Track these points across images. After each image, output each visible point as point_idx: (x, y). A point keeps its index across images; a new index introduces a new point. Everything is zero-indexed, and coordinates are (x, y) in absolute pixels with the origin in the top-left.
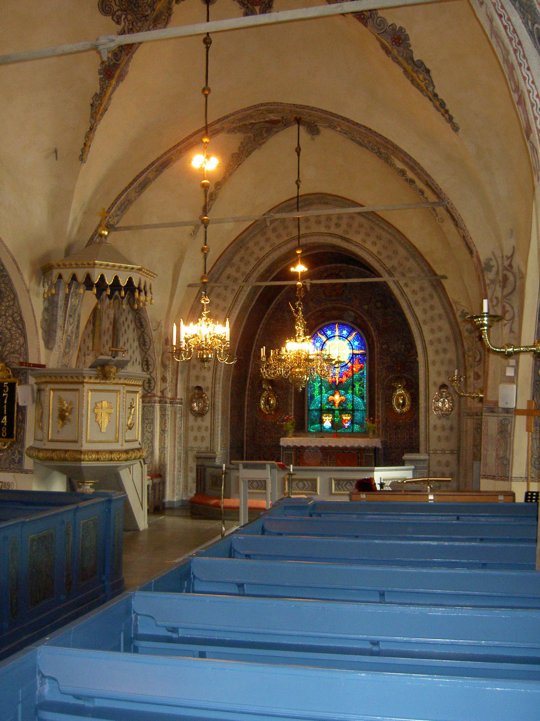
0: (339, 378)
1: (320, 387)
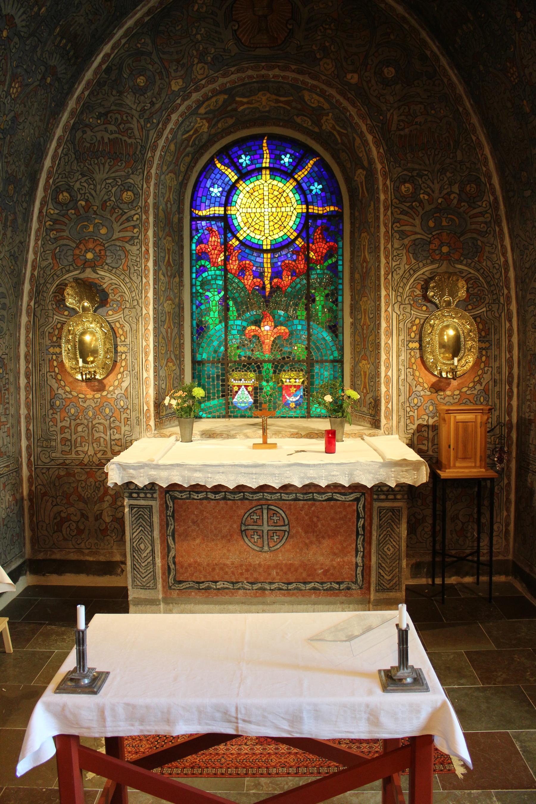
0: (271, 279)
1: (225, 299)
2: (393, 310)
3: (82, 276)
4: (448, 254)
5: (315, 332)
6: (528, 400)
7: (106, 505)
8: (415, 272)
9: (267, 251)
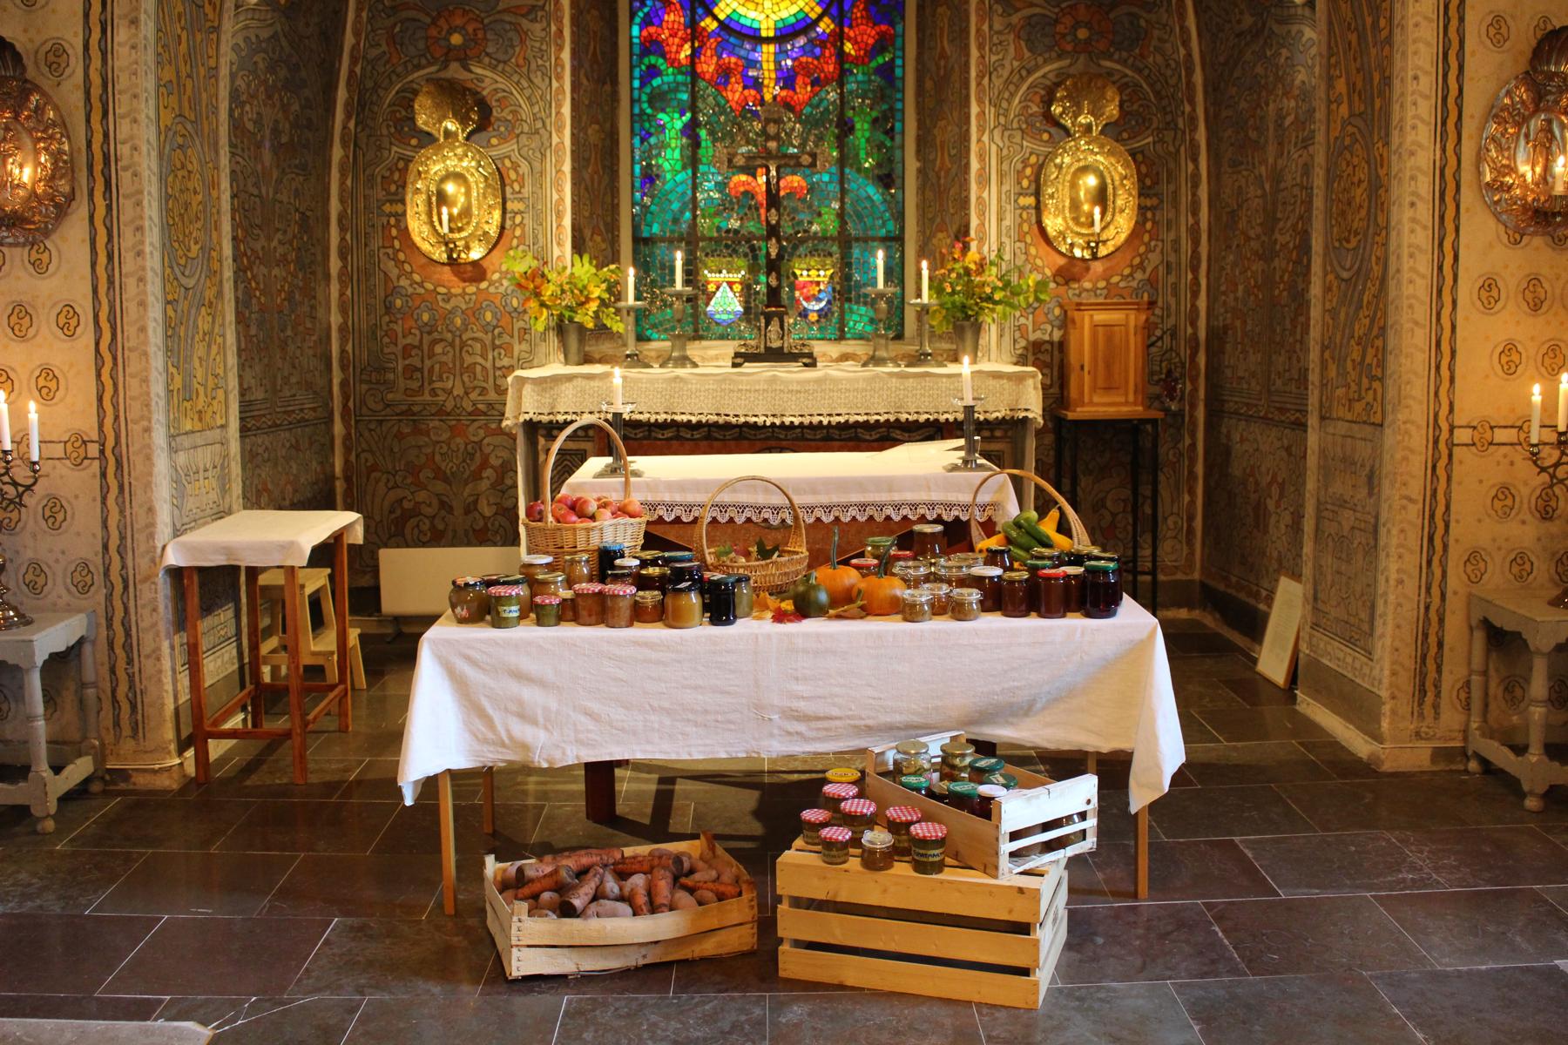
1: (690, 130)
2: (992, 139)
3: (443, 75)
4: (1088, 41)
5: (854, 186)
6: (1224, 293)
7: (484, 485)
8: (1029, 73)
9: (768, 40)
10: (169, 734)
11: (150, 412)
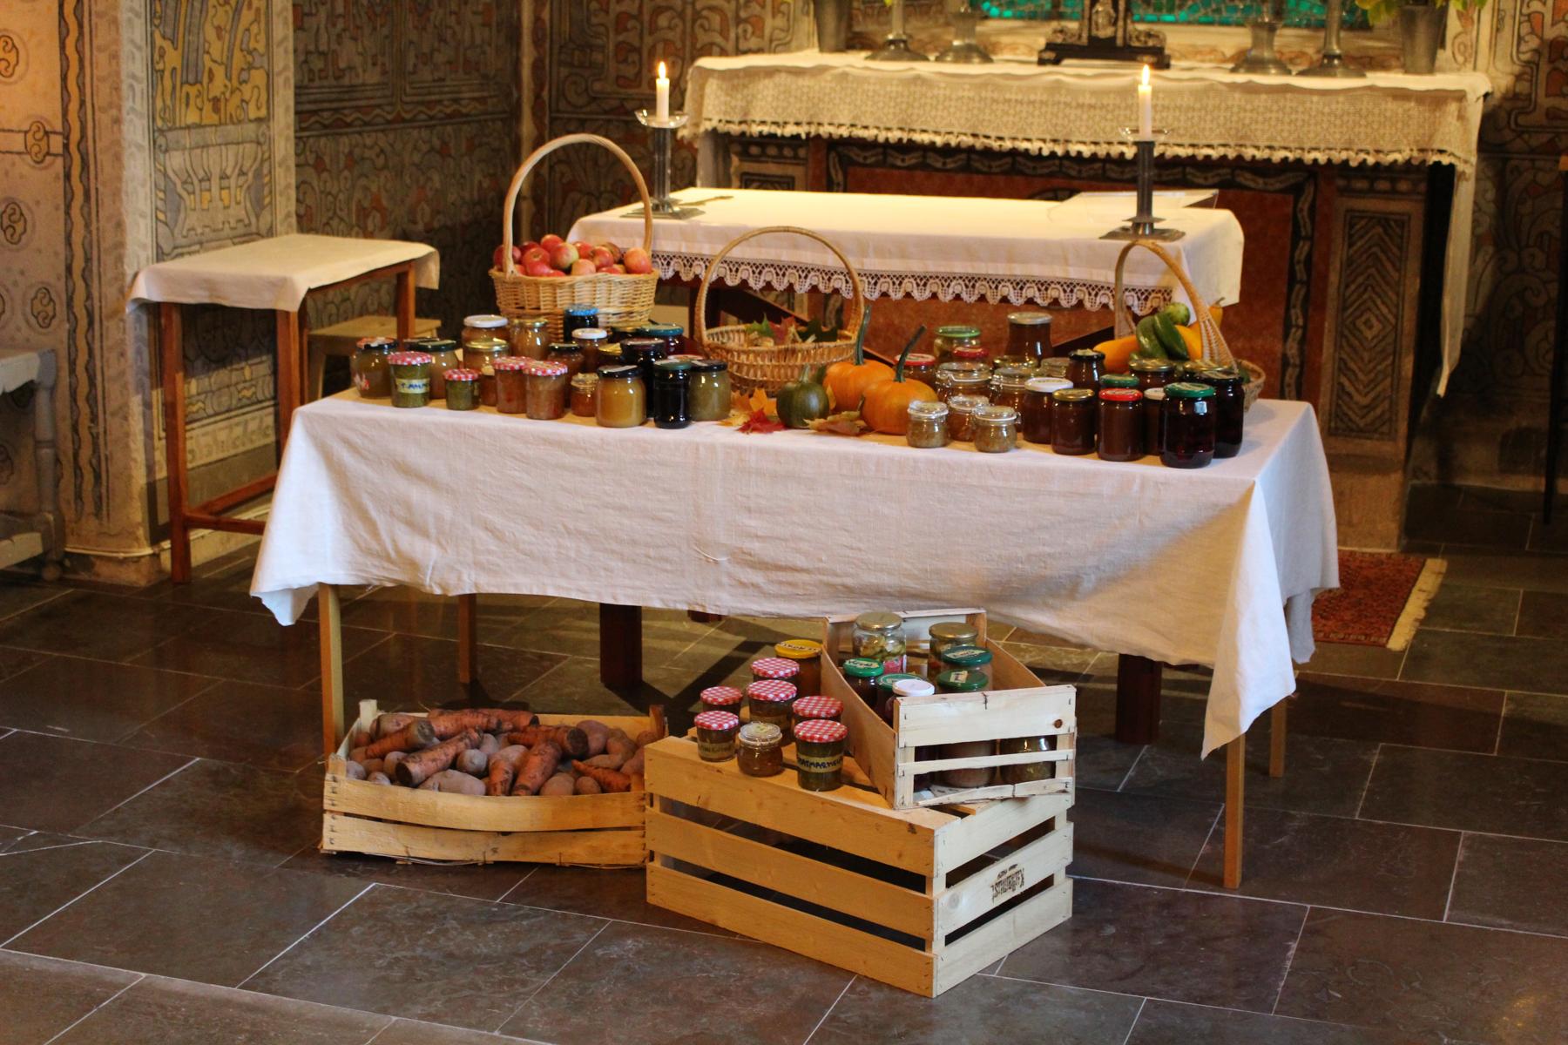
10: (137, 513)
11: (120, 98)
